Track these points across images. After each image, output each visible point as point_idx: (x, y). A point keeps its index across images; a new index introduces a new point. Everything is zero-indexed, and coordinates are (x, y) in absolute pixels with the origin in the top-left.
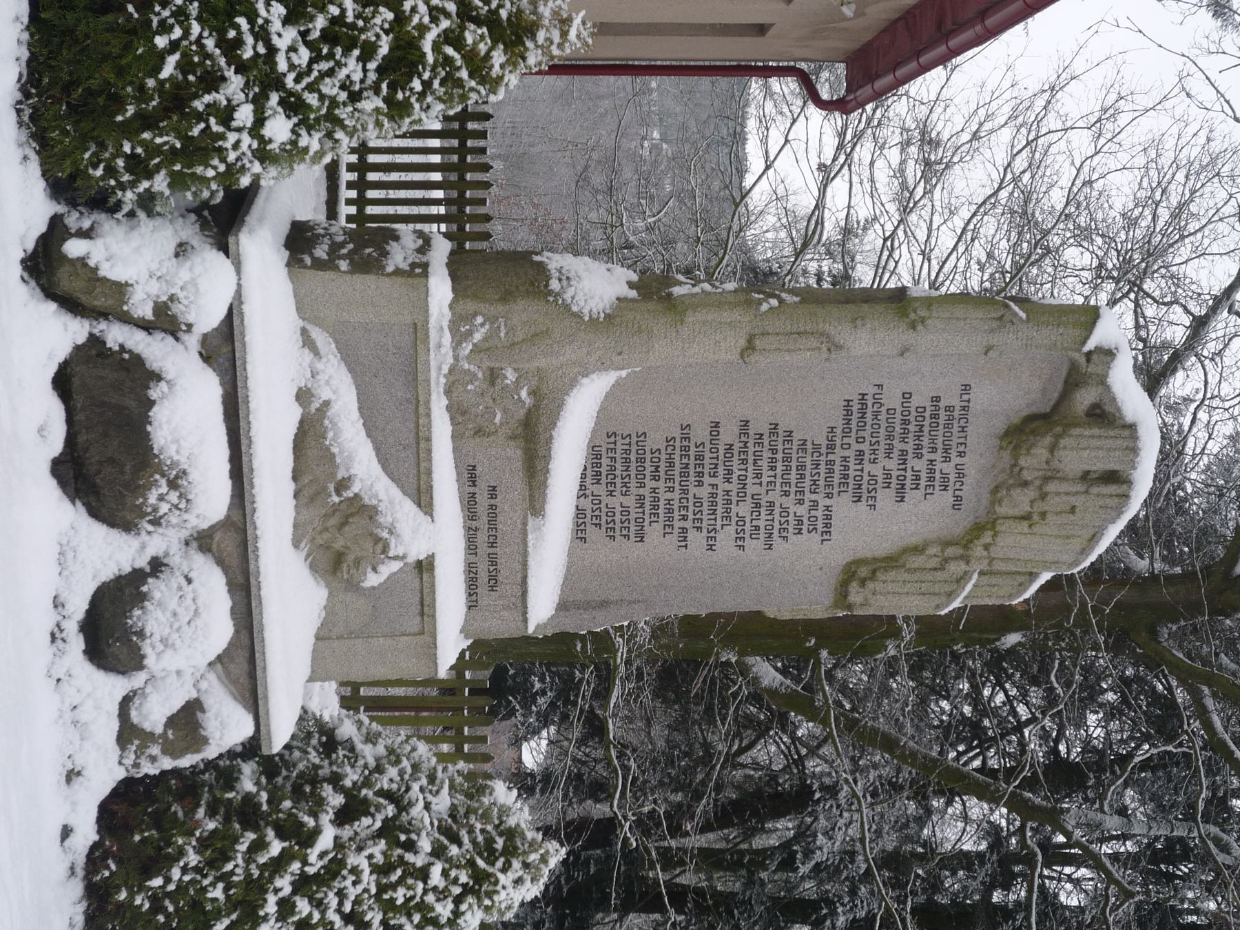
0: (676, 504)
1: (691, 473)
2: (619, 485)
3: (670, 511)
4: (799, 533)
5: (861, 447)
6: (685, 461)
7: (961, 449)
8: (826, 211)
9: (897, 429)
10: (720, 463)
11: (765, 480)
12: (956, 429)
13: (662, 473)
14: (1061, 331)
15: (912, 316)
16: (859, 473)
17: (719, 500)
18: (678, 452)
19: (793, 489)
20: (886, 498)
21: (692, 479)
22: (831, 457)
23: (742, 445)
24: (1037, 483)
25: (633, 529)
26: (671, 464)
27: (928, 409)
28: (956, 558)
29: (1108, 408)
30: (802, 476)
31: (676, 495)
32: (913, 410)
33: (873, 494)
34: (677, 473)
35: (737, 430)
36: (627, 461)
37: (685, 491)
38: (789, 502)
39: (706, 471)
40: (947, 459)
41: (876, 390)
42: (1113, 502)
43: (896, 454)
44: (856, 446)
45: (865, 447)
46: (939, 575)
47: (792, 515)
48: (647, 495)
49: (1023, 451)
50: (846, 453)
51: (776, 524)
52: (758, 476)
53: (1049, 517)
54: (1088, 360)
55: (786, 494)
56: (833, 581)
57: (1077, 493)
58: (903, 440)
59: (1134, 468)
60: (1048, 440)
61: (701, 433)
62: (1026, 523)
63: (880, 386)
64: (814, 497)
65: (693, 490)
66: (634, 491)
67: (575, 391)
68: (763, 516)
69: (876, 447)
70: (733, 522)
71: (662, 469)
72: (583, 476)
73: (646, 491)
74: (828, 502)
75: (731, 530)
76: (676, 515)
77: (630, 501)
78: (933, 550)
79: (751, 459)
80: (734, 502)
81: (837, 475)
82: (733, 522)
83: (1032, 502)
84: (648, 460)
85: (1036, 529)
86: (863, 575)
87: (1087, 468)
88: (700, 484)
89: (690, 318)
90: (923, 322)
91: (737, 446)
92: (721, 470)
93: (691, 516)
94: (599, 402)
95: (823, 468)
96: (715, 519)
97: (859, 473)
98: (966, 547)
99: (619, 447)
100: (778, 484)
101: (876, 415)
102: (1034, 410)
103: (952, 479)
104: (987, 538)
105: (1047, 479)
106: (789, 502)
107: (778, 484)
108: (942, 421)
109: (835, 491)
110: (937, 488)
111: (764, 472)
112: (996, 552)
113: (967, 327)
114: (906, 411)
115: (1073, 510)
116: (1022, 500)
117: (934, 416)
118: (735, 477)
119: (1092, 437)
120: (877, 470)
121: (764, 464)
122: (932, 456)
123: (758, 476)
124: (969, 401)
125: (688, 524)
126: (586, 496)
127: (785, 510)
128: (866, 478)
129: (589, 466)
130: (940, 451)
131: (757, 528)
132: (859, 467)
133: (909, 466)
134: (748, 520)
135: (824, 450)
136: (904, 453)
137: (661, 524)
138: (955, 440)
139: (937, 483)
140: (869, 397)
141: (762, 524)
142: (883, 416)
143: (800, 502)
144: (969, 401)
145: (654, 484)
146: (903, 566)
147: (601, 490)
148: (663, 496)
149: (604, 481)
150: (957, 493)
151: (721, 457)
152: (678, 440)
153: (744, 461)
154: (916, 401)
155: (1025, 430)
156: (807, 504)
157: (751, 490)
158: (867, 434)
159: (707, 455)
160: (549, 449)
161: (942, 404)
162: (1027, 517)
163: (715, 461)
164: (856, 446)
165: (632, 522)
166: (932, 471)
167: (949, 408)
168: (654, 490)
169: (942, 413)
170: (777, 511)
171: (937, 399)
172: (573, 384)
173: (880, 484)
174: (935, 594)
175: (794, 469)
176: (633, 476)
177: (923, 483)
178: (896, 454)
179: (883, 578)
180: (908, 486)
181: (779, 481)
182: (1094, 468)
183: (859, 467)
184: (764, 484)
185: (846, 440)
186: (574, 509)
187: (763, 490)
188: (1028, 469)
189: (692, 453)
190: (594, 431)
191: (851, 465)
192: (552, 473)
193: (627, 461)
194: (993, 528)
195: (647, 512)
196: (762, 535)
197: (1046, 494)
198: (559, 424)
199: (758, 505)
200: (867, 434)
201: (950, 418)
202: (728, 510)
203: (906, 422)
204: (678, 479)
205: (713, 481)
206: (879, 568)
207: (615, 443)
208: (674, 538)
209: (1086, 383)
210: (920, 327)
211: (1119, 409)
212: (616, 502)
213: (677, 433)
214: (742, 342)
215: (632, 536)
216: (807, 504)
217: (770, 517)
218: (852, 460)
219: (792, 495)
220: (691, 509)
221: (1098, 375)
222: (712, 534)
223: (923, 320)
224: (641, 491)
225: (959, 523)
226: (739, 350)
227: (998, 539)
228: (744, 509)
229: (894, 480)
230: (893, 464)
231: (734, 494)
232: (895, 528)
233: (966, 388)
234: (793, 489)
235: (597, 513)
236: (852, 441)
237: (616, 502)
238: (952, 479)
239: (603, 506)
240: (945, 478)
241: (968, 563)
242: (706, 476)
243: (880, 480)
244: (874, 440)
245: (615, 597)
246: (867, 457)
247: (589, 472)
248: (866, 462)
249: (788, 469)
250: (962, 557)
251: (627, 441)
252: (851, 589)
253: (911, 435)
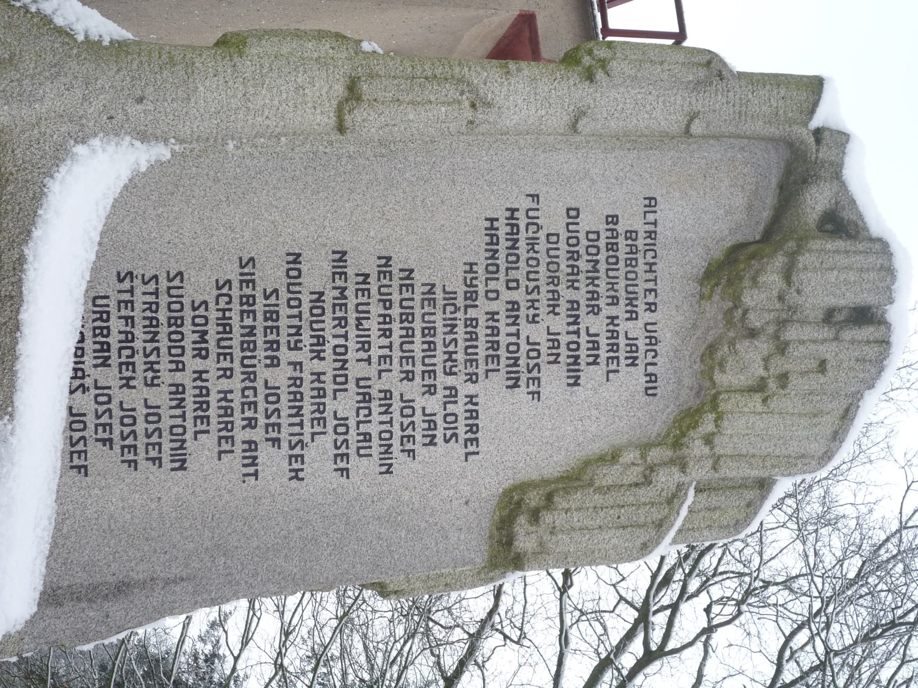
0: (237, 399)
1: (260, 343)
2: (140, 367)
3: (228, 411)
4: (432, 443)
5: (515, 296)
6: (248, 322)
7: (651, 298)
8: (187, 638)
9: (563, 267)
10: (305, 325)
11: (375, 353)
12: (641, 268)
13: (212, 345)
14: (783, 92)
15: (587, 60)
16: (513, 339)
17: (306, 389)
18: (236, 306)
19: (419, 368)
20: (553, 378)
21: (261, 353)
22: (472, 313)
23: (336, 293)
24: (771, 329)
25: (167, 446)
26: (225, 326)
27: (603, 235)
28: (664, 464)
29: (846, 215)
30: (431, 346)
31: (236, 383)
32: (582, 236)
33: (535, 374)
34: (236, 343)
35: (328, 269)
36: (153, 322)
37: (250, 376)
38: (414, 390)
39: (283, 339)
40: (633, 316)
41: (528, 203)
42: (871, 352)
43: (563, 309)
44: (507, 295)
45: (519, 296)
46: (644, 494)
47: (419, 412)
48: (189, 384)
49: (746, 283)
50: (494, 306)
51: (396, 427)
52: (365, 346)
53: (794, 380)
54: (818, 141)
55: (409, 376)
56: (486, 523)
57: (825, 340)
58: (572, 286)
59: (891, 301)
60: (780, 260)
61: (271, 275)
62: (758, 397)
63: (535, 197)
64: (450, 381)
65: (263, 373)
66: (166, 377)
67: (63, 169)
68: (376, 417)
69: (534, 296)
70: (330, 429)
71: (212, 338)
72: (79, 352)
73: (185, 378)
74: (471, 389)
75: (326, 441)
76: (237, 418)
77: (161, 396)
78: (629, 456)
79: (352, 316)
80: (329, 393)
81: (482, 343)
82: (330, 429)
83: (766, 360)
84: (188, 321)
85: (773, 404)
86: (533, 504)
87: (831, 301)
88: (274, 362)
89: (253, 50)
90: (603, 67)
91: (330, 295)
92: (306, 338)
93: (262, 421)
94: (103, 214)
95: (460, 329)
96: (301, 424)
97: (513, 339)
98: (677, 444)
99: (139, 299)
100: (396, 361)
101: (532, 243)
102: (739, 238)
103: (642, 348)
104: (707, 425)
105: (782, 324)
106: (414, 390)
107: (396, 361)
108: (622, 255)
109: (481, 370)
110: (623, 362)
111: (373, 339)
112: (723, 445)
113: (665, 76)
114: (573, 239)
115: (822, 366)
116: (751, 359)
117: (612, 247)
118: (328, 348)
119: (837, 252)
120: (538, 334)
121: (373, 325)
122: (613, 311)
123: (365, 346)
124: (655, 223)
125: (258, 435)
126: (84, 389)
127: (408, 404)
128: (524, 348)
129: (89, 334)
130: (623, 302)
131: (367, 437)
132: (513, 329)
133: (582, 326)
134: (352, 423)
135: (460, 302)
136: (574, 305)
137: (214, 436)
138: (642, 286)
139: (622, 354)
140: (520, 215)
141: (373, 429)
142: (542, 246)
143: (431, 390)
144: (655, 223)
145: (199, 364)
146: (591, 484)
147: (110, 377)
148: (216, 385)
149: (114, 360)
150: (650, 369)
151: (306, 315)
152: (236, 284)
153: (342, 322)
154: (587, 222)
155: (728, 269)
156: (441, 393)
157: (355, 370)
158: (520, 275)
159: (284, 311)
160: (19, 283)
161: (621, 228)
162: (760, 387)
163: (295, 322)
164: (507, 295)
165: (165, 434)
166: (614, 335)
167: (631, 235)
168: (200, 375)
169: (621, 240)
170: (396, 405)
171: (613, 219)
172: (59, 155)
173: (544, 358)
174: (639, 526)
175: (418, 333)
176: (164, 350)
177: (603, 354)
178: (563, 309)
179: (565, 505)
180: (583, 360)
181: (397, 354)
182: (842, 302)
183: (513, 329)
184: (374, 360)
185: (492, 285)
186: (64, 413)
187: (372, 371)
188: (755, 309)
189: (259, 307)
190: (96, 269)
191: (501, 325)
192: (26, 330)
193: (153, 322)
194: (714, 406)
195: (190, 415)
196: (376, 450)
197: (787, 344)
198: (37, 233)
199: (366, 398)
200: (520, 275)
201: (633, 249)
202: (320, 408)
203: (574, 256)
204: (237, 353)
205: (295, 356)
206: (557, 490)
207: (131, 291)
208: (234, 461)
209: (817, 177)
210: (600, 75)
211: (860, 216)
212: (135, 398)
213: (233, 273)
214: (340, 89)
215: (166, 458)
216: (441, 393)
217: (386, 418)
218: (502, 317)
219: (418, 379)
220: (261, 406)
221: (831, 164)
222: (297, 451)
223: (603, 64)
224: (179, 377)
225: (656, 417)
226: (335, 103)
227: (725, 423)
228: (344, 405)
229: (563, 350)
230: (559, 324)
231: (328, 378)
232: (570, 429)
233: (651, 203)
234: (419, 368)
235: (105, 419)
236: (500, 286)
237: (135, 398)
238: (642, 348)
239: (114, 406)
240: (632, 346)
241: (683, 468)
242: (284, 348)
243: (544, 350)
244: (532, 285)
245: (139, 575)
246: (523, 312)
247: (89, 345)
248: (522, 321)
249: (409, 334)
250: (672, 462)
251: (151, 287)
252: (517, 529)
253: (582, 277)
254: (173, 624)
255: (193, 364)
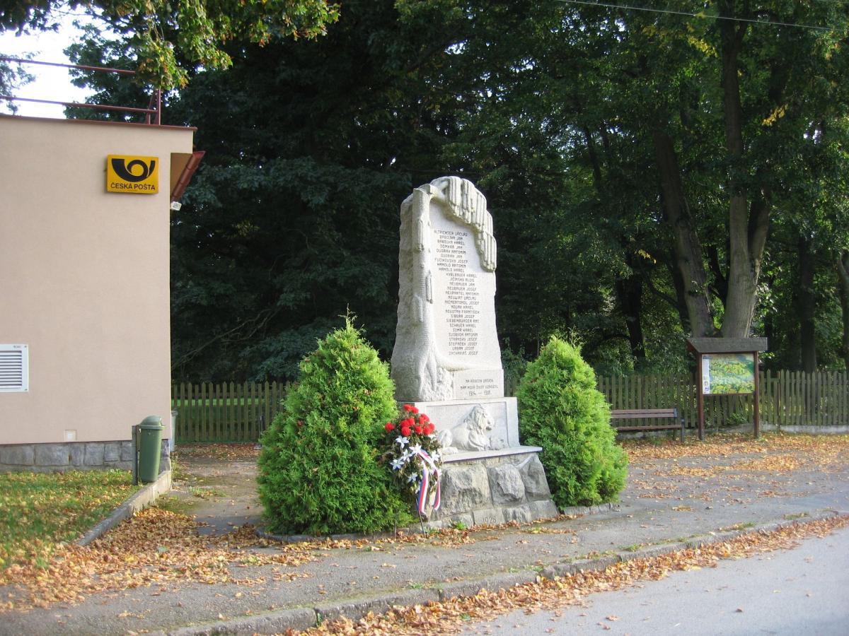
38: (466, 287)
65: (463, 318)
77: (467, 337)
120: (457, 260)
121: (457, 296)
127: (468, 289)
147: (464, 347)
148: (465, 327)
157: (463, 300)
171: (438, 251)
208: (476, 324)
212: (467, 342)
228: (468, 301)
230: (456, 255)
237: (467, 342)
254: (454, 47)
255: (462, 332)
